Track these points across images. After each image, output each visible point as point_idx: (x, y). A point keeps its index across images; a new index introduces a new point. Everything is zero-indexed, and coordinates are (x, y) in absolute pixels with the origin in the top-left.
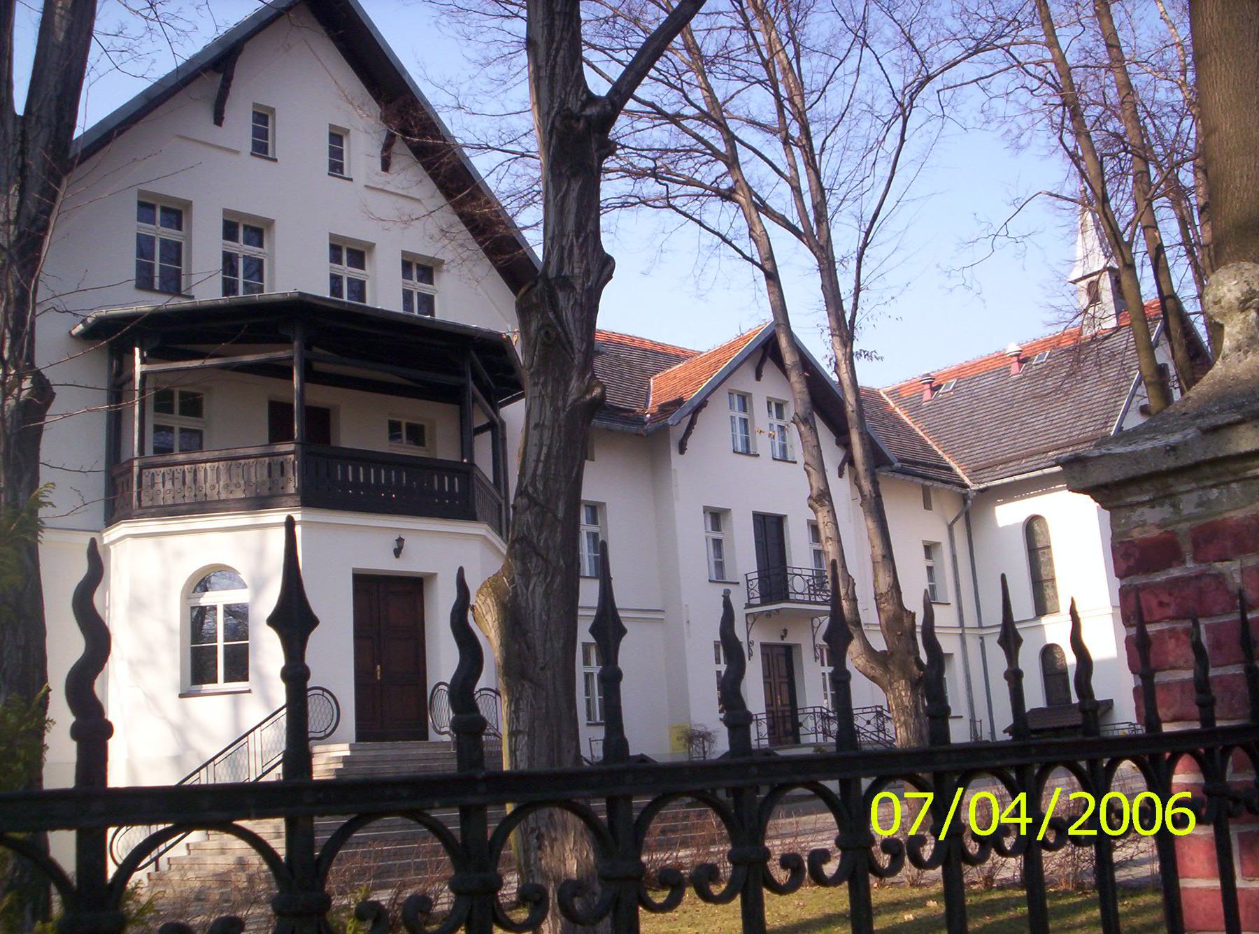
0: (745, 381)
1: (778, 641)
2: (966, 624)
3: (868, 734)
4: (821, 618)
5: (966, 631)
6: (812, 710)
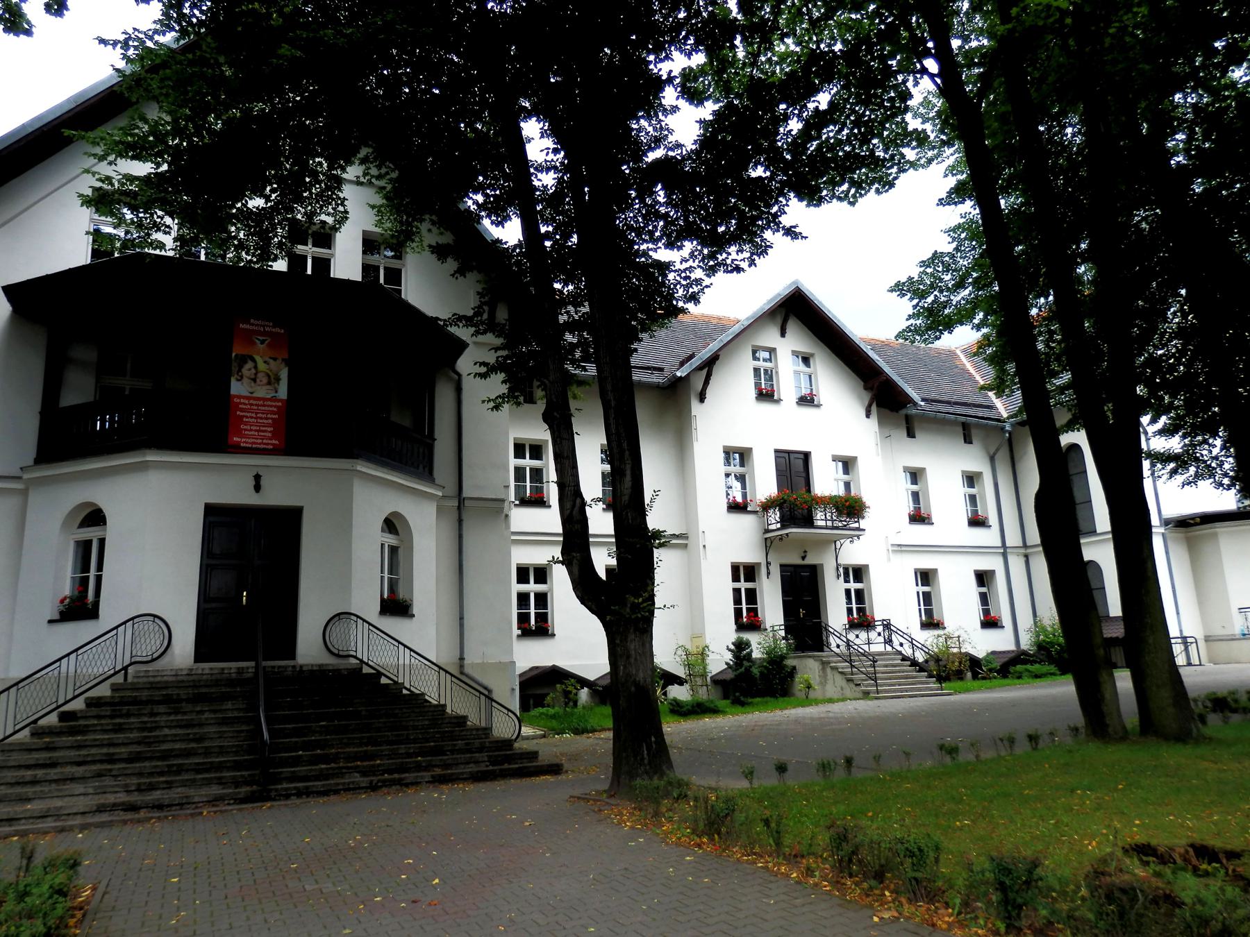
0: (770, 337)
1: (800, 562)
2: (1008, 544)
3: (856, 647)
4: (842, 541)
5: (1008, 550)
6: (880, 623)
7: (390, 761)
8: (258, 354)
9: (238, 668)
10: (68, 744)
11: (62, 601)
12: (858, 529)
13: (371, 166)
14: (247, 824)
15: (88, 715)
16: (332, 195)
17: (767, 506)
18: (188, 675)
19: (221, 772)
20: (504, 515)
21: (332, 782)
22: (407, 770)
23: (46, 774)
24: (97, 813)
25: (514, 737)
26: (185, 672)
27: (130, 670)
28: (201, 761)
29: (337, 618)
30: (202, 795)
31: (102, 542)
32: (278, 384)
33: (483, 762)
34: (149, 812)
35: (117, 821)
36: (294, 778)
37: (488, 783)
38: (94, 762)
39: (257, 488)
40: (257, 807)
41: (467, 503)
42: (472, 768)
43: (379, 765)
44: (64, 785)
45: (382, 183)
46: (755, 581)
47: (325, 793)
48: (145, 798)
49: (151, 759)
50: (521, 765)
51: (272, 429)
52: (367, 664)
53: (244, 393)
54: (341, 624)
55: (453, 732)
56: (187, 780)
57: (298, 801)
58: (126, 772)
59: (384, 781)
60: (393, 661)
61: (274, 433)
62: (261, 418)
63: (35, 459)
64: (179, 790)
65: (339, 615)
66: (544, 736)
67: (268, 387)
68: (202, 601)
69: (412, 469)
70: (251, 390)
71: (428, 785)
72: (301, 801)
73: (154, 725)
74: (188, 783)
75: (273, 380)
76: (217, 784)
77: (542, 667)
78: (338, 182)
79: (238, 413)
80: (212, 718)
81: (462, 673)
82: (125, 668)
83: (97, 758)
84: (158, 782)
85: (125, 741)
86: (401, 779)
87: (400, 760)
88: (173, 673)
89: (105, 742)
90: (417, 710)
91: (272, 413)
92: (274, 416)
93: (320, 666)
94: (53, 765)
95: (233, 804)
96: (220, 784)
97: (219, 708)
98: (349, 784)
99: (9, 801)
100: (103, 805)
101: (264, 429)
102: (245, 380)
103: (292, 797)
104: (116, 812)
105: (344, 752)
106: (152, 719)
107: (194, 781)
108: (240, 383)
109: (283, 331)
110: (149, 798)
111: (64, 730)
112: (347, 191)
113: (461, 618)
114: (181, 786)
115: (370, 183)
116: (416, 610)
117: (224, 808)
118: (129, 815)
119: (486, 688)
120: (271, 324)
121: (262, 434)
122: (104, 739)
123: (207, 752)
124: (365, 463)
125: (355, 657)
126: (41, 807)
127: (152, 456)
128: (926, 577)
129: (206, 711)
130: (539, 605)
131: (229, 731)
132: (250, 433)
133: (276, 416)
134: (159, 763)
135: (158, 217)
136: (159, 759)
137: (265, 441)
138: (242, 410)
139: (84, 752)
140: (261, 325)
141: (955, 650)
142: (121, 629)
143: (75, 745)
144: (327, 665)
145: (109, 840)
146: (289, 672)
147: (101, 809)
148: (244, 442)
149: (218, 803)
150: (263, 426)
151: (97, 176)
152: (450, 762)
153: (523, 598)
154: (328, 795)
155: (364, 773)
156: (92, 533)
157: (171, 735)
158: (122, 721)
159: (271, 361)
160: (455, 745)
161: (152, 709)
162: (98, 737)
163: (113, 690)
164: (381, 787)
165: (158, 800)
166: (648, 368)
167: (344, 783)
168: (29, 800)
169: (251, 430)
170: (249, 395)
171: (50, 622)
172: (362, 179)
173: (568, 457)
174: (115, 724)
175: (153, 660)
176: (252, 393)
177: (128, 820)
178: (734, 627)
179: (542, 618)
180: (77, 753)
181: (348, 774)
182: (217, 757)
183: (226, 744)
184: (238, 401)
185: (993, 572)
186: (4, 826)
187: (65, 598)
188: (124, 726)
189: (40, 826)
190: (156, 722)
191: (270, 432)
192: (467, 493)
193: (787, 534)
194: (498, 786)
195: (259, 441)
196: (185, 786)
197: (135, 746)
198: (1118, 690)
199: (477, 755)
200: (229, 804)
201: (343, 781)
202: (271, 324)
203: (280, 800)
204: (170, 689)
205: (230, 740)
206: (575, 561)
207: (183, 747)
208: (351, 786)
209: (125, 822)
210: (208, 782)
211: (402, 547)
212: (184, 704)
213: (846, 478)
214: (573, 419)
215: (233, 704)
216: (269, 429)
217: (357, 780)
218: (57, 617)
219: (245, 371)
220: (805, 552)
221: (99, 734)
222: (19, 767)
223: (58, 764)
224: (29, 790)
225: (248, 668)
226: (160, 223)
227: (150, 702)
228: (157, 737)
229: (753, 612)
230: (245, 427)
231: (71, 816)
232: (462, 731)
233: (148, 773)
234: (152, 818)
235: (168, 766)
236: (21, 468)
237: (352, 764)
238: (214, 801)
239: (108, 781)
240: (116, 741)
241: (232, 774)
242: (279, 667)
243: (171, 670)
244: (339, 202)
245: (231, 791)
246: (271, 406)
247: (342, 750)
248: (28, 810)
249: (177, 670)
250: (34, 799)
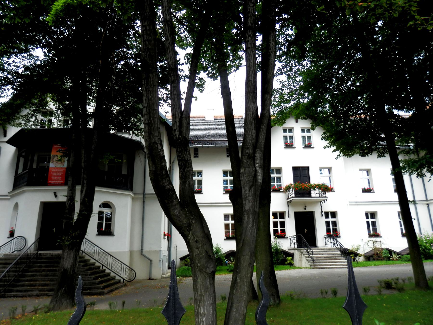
1: (304, 210)
12: (325, 197)
17: (288, 188)
39: (56, 196)
41: (146, 196)
46: (284, 219)
52: (84, 252)
60: (93, 251)
61: (62, 179)
65: (22, 237)
67: (61, 164)
70: (55, 165)
91: (62, 172)
102: (54, 163)
113: (143, 235)
127: (26, 188)
128: (373, 215)
133: (62, 173)
137: (59, 181)
138: (53, 172)
141: (379, 247)
153: (327, 223)
164: (40, 296)
166: (220, 141)
178: (368, 236)
179: (335, 230)
185: (285, 212)
193: (292, 200)
195: (57, 181)
198: (354, 272)
213: (368, 177)
220: (306, 206)
229: (375, 230)
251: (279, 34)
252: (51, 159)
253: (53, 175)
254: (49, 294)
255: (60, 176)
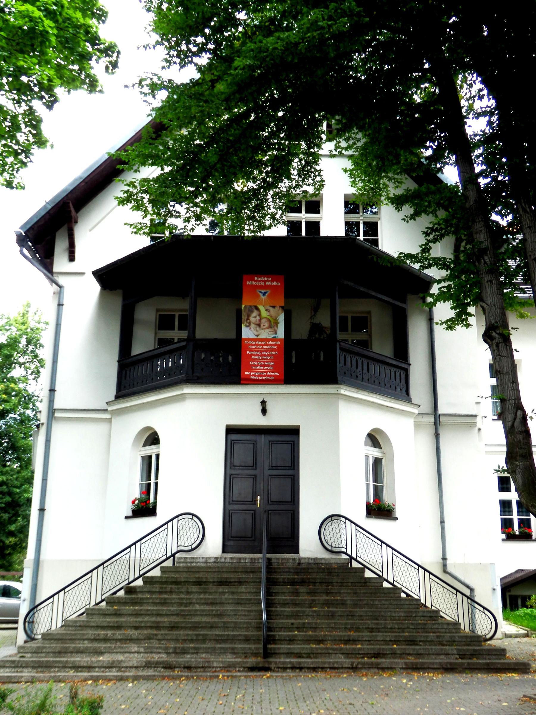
7: (369, 647)
8: (261, 304)
9: (251, 559)
10: (130, 612)
11: (133, 502)
13: (341, 140)
14: (245, 689)
15: (144, 590)
16: (311, 169)
18: (214, 562)
19: (235, 644)
20: (477, 429)
21: (320, 660)
22: (384, 655)
23: (114, 634)
24: (146, 668)
25: (488, 637)
26: (212, 560)
27: (177, 555)
28: (220, 633)
29: (329, 519)
30: (219, 661)
31: (158, 456)
32: (277, 327)
33: (453, 654)
34: (181, 671)
35: (158, 676)
36: (289, 654)
37: (457, 675)
38: (146, 628)
39: (264, 411)
40: (260, 676)
41: (442, 419)
42: (443, 659)
43: (360, 649)
44: (125, 644)
45: (350, 152)
47: (314, 669)
48: (178, 660)
49: (185, 628)
50: (489, 661)
51: (273, 363)
52: (356, 560)
53: (252, 336)
54: (333, 525)
55: (425, 624)
56: (209, 648)
57: (292, 674)
58: (167, 637)
59: (364, 664)
61: (275, 369)
62: (265, 355)
63: (115, 396)
64: (204, 655)
65: (193, 515)
66: (527, 635)
68: (227, 503)
69: (390, 391)
70: (257, 333)
71: (402, 671)
72: (294, 674)
73: (188, 601)
74: (210, 651)
75: (273, 324)
76: (230, 653)
77: (527, 570)
78: (316, 158)
79: (248, 352)
80: (230, 599)
81: (445, 571)
82: (173, 555)
83: (148, 625)
84: (189, 648)
85: (168, 613)
86: (378, 664)
87: (378, 647)
88: (204, 560)
89: (154, 612)
90: (395, 603)
92: (274, 353)
93: (315, 559)
94: (119, 627)
95: (243, 671)
96: (234, 653)
97: (236, 590)
98: (333, 663)
99: (89, 653)
100: (149, 662)
101: (267, 364)
102: (252, 326)
103: (288, 670)
104: (159, 669)
105: (331, 636)
106: (188, 597)
107: (214, 649)
108: (248, 328)
109: (279, 284)
110: (181, 660)
111: (128, 601)
112: (324, 164)
113: (442, 522)
114: (205, 653)
115: (341, 155)
116: (398, 513)
117: (234, 674)
118: (167, 673)
119: (468, 587)
120: (270, 279)
121: (266, 368)
122: (153, 610)
123: (225, 627)
124: (348, 388)
125: (346, 553)
126: (109, 659)
127: (188, 390)
129: (226, 592)
130: (521, 514)
131: (242, 610)
132: (257, 368)
133: (277, 353)
134: (191, 632)
135: (171, 206)
136: (190, 628)
137: (268, 374)
138: (251, 350)
139: (140, 619)
140: (263, 281)
142: (170, 524)
143: (134, 613)
144: (322, 559)
145: (147, 690)
146: (290, 564)
147: (148, 665)
148: (252, 375)
149: (230, 669)
150: (267, 362)
151: (125, 183)
152: (422, 652)
154: (316, 672)
155: (347, 655)
156: (151, 450)
157: (200, 610)
158: (166, 596)
159: (271, 309)
160: (427, 637)
161: (188, 588)
162: (150, 608)
163: (162, 572)
165: (188, 662)
167: (329, 663)
168: (101, 653)
169: (258, 365)
170: (256, 337)
171: (127, 517)
172: (334, 152)
173: (507, 373)
174: (161, 599)
175: (193, 550)
176: (257, 336)
177: (166, 676)
180: (135, 620)
181: (333, 655)
182: (233, 631)
183: (239, 621)
184: (248, 343)
186: (85, 672)
187: (135, 500)
188: (168, 601)
189: (107, 674)
190: (190, 599)
191: (272, 366)
192: (441, 411)
194: (462, 678)
196: (208, 653)
197: (174, 617)
199: (447, 647)
200: (239, 671)
201: (328, 660)
202: (270, 279)
203: (278, 672)
204: (202, 573)
205: (242, 617)
206: (518, 470)
207: (208, 620)
208: (335, 665)
209: (163, 678)
210: (224, 651)
211: (384, 459)
212: (211, 586)
214: (511, 337)
215: (246, 588)
216: (271, 364)
217: (340, 660)
218: (130, 514)
219: (252, 319)
221: (150, 606)
222: (98, 627)
223: (122, 627)
224: (102, 646)
225: (258, 559)
226: (172, 210)
227: (187, 582)
228: (189, 611)
230: (253, 363)
231: (128, 669)
232: (434, 624)
233: (183, 640)
234: (182, 676)
235: (197, 635)
236: (107, 403)
237: (338, 646)
238: (228, 667)
239: (155, 643)
240: (161, 612)
241: (242, 646)
242: (283, 559)
243: (203, 558)
244: (317, 173)
245: (241, 660)
246: (272, 345)
247: (329, 633)
248: (100, 661)
249: (207, 558)
250: (105, 652)
251: (174, 48)
252: (244, 317)
253: (253, 357)
254: (384, 666)
255: (271, 361)
